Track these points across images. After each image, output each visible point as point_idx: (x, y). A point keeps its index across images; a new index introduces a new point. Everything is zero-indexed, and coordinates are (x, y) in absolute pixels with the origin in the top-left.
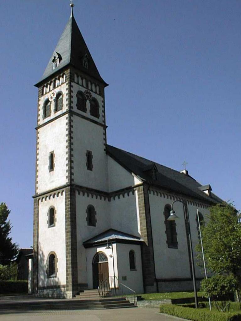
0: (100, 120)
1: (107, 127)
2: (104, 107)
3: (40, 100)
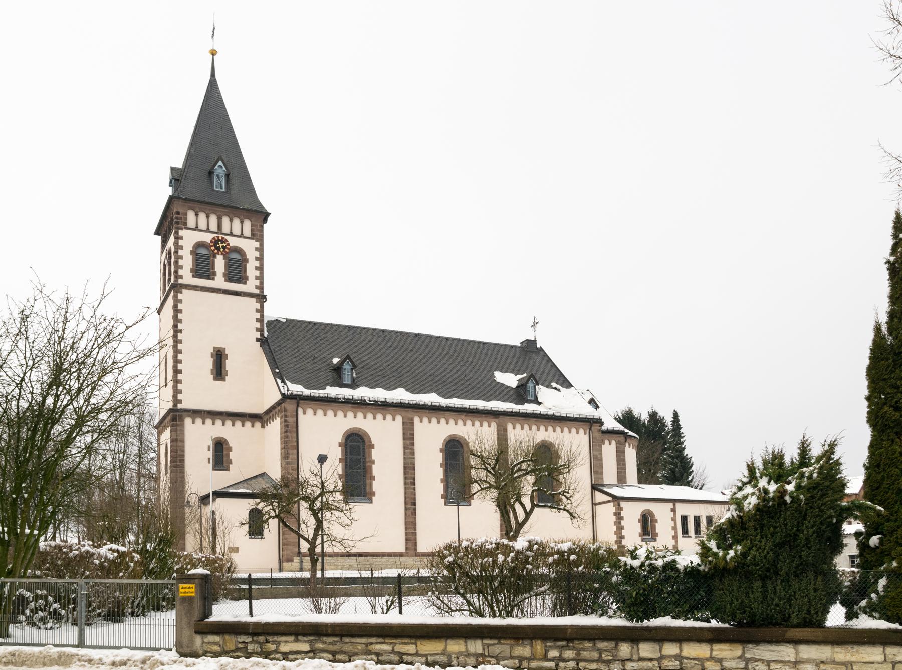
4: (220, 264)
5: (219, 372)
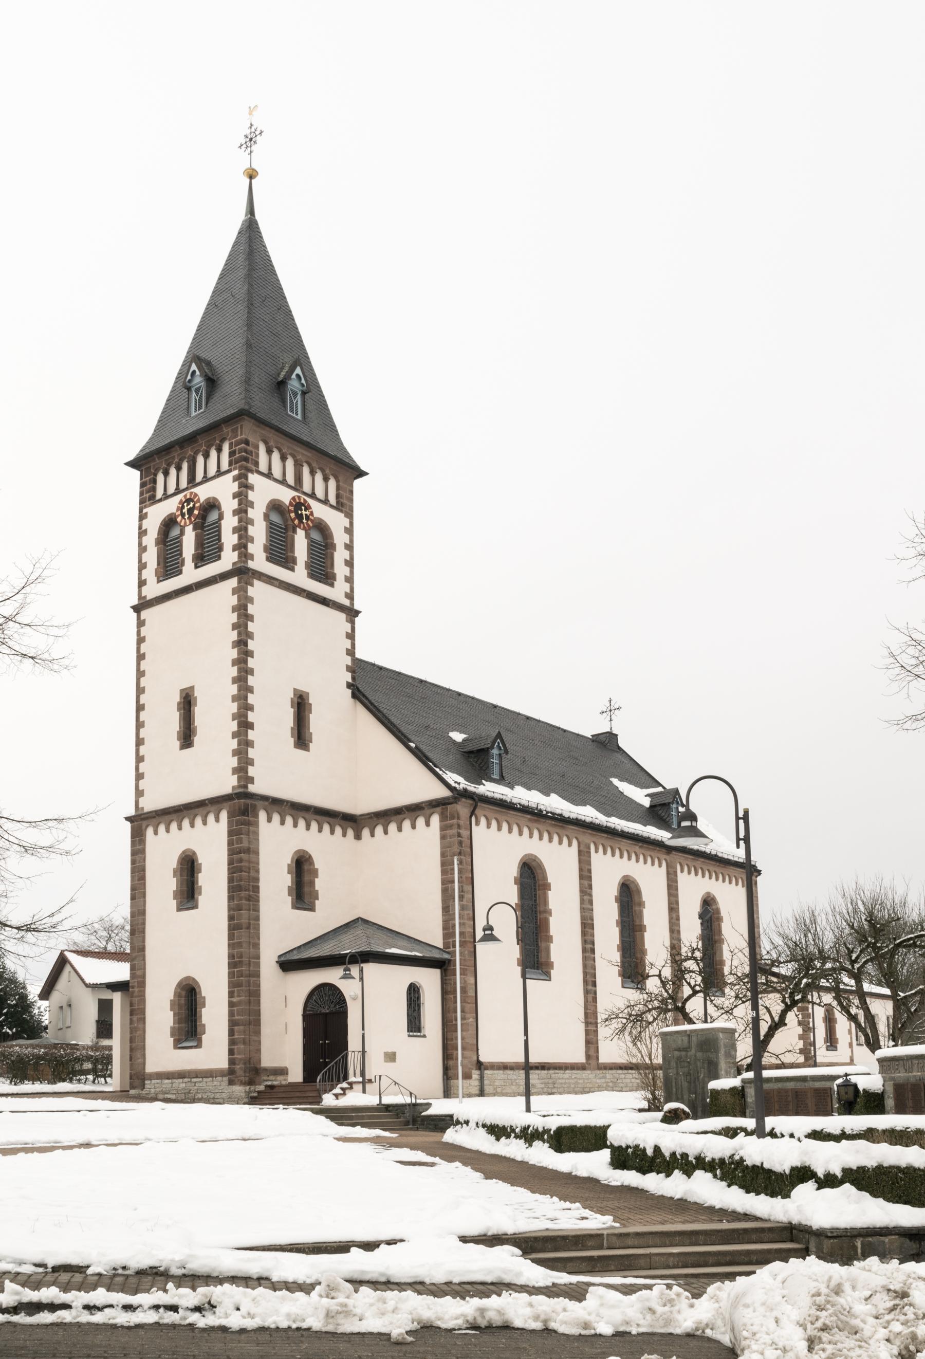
0: (337, 593)
1: (357, 613)
2: (349, 547)
3: (146, 513)
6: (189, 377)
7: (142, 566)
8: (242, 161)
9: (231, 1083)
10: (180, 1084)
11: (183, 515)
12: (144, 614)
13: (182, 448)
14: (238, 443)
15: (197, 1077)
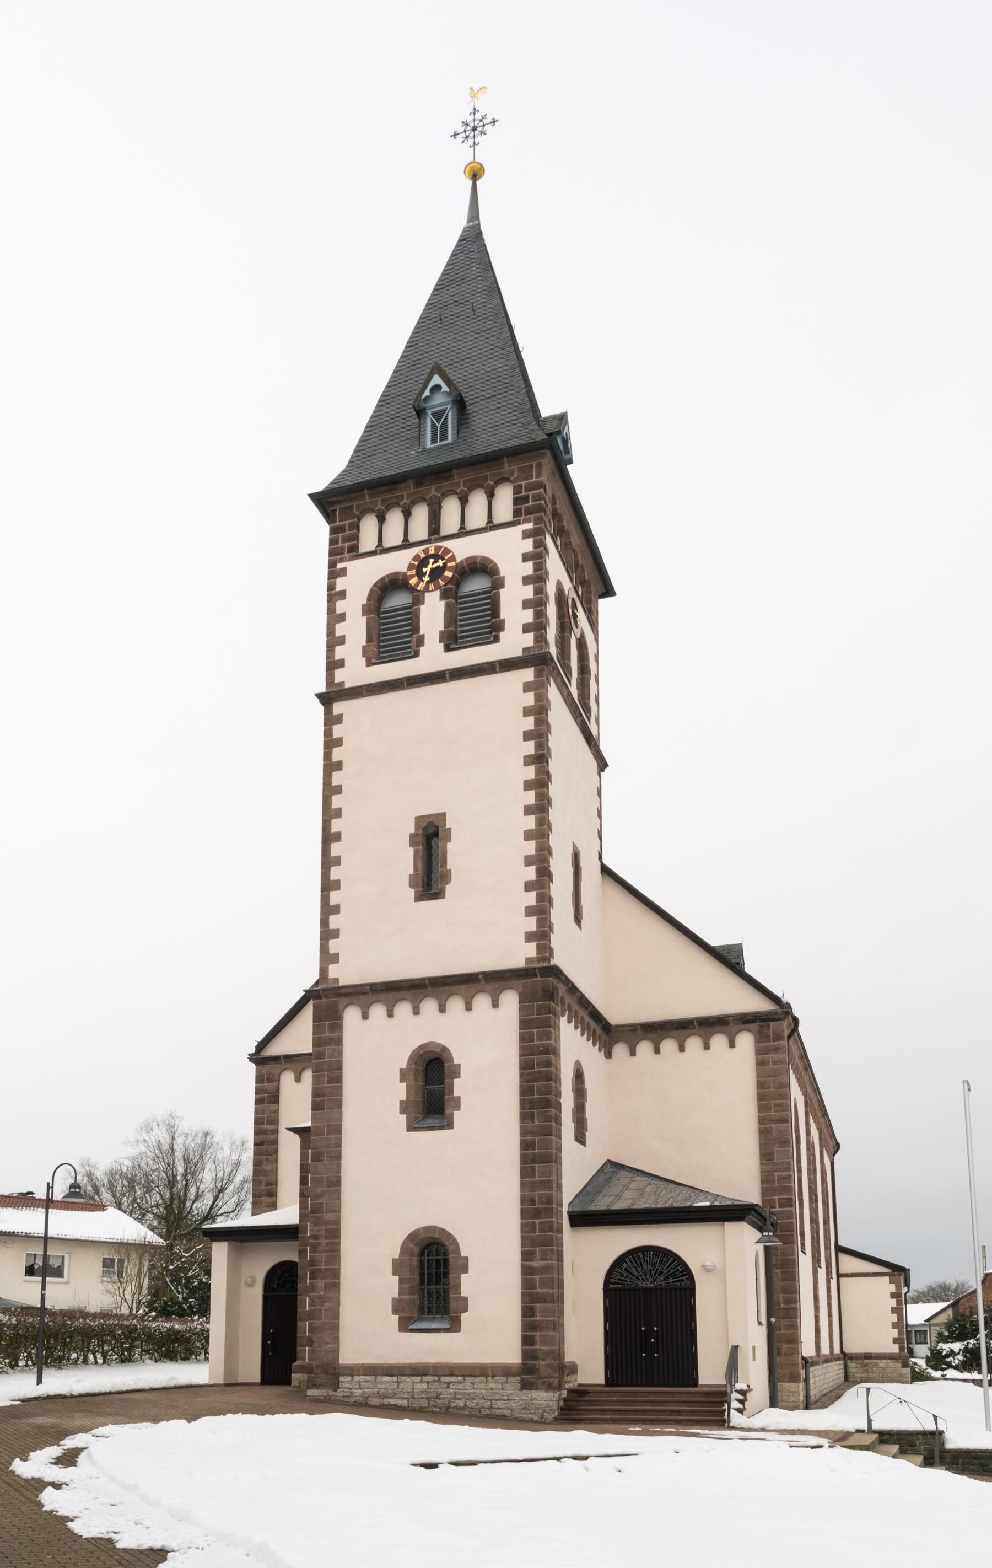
4: (433, 613)
5: (430, 880)
6: (427, 393)
7: (334, 641)
8: (463, 154)
9: (526, 1386)
10: (419, 1385)
11: (420, 575)
12: (338, 708)
13: (418, 484)
14: (530, 488)
15: (452, 1375)
